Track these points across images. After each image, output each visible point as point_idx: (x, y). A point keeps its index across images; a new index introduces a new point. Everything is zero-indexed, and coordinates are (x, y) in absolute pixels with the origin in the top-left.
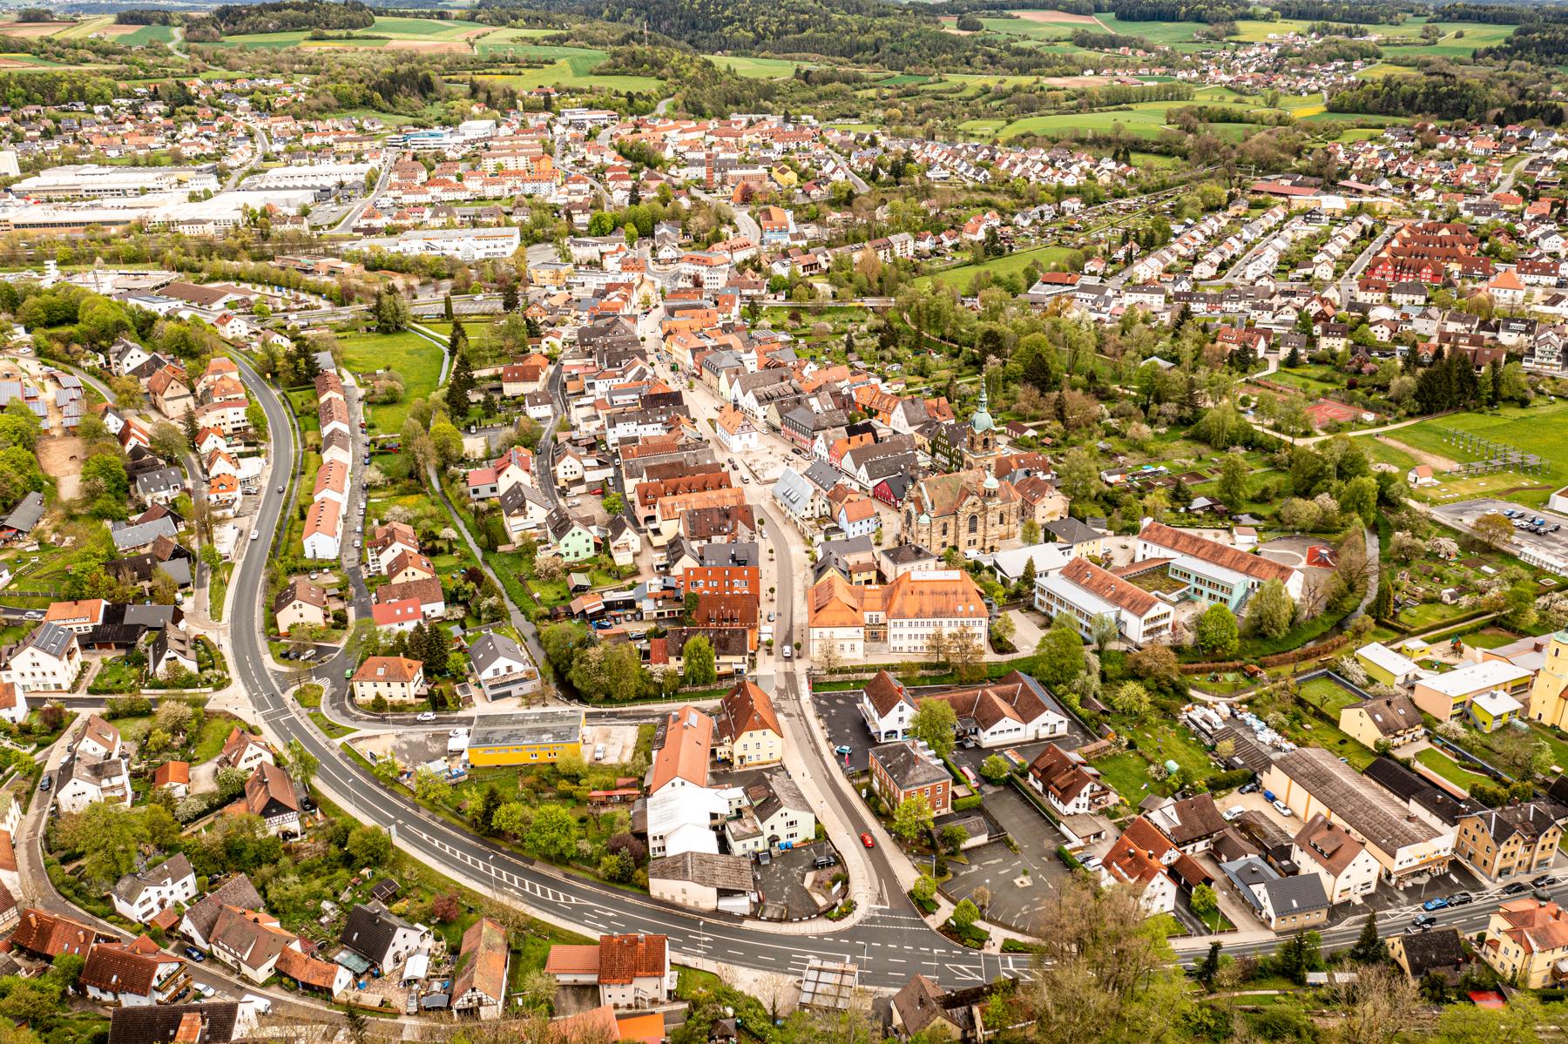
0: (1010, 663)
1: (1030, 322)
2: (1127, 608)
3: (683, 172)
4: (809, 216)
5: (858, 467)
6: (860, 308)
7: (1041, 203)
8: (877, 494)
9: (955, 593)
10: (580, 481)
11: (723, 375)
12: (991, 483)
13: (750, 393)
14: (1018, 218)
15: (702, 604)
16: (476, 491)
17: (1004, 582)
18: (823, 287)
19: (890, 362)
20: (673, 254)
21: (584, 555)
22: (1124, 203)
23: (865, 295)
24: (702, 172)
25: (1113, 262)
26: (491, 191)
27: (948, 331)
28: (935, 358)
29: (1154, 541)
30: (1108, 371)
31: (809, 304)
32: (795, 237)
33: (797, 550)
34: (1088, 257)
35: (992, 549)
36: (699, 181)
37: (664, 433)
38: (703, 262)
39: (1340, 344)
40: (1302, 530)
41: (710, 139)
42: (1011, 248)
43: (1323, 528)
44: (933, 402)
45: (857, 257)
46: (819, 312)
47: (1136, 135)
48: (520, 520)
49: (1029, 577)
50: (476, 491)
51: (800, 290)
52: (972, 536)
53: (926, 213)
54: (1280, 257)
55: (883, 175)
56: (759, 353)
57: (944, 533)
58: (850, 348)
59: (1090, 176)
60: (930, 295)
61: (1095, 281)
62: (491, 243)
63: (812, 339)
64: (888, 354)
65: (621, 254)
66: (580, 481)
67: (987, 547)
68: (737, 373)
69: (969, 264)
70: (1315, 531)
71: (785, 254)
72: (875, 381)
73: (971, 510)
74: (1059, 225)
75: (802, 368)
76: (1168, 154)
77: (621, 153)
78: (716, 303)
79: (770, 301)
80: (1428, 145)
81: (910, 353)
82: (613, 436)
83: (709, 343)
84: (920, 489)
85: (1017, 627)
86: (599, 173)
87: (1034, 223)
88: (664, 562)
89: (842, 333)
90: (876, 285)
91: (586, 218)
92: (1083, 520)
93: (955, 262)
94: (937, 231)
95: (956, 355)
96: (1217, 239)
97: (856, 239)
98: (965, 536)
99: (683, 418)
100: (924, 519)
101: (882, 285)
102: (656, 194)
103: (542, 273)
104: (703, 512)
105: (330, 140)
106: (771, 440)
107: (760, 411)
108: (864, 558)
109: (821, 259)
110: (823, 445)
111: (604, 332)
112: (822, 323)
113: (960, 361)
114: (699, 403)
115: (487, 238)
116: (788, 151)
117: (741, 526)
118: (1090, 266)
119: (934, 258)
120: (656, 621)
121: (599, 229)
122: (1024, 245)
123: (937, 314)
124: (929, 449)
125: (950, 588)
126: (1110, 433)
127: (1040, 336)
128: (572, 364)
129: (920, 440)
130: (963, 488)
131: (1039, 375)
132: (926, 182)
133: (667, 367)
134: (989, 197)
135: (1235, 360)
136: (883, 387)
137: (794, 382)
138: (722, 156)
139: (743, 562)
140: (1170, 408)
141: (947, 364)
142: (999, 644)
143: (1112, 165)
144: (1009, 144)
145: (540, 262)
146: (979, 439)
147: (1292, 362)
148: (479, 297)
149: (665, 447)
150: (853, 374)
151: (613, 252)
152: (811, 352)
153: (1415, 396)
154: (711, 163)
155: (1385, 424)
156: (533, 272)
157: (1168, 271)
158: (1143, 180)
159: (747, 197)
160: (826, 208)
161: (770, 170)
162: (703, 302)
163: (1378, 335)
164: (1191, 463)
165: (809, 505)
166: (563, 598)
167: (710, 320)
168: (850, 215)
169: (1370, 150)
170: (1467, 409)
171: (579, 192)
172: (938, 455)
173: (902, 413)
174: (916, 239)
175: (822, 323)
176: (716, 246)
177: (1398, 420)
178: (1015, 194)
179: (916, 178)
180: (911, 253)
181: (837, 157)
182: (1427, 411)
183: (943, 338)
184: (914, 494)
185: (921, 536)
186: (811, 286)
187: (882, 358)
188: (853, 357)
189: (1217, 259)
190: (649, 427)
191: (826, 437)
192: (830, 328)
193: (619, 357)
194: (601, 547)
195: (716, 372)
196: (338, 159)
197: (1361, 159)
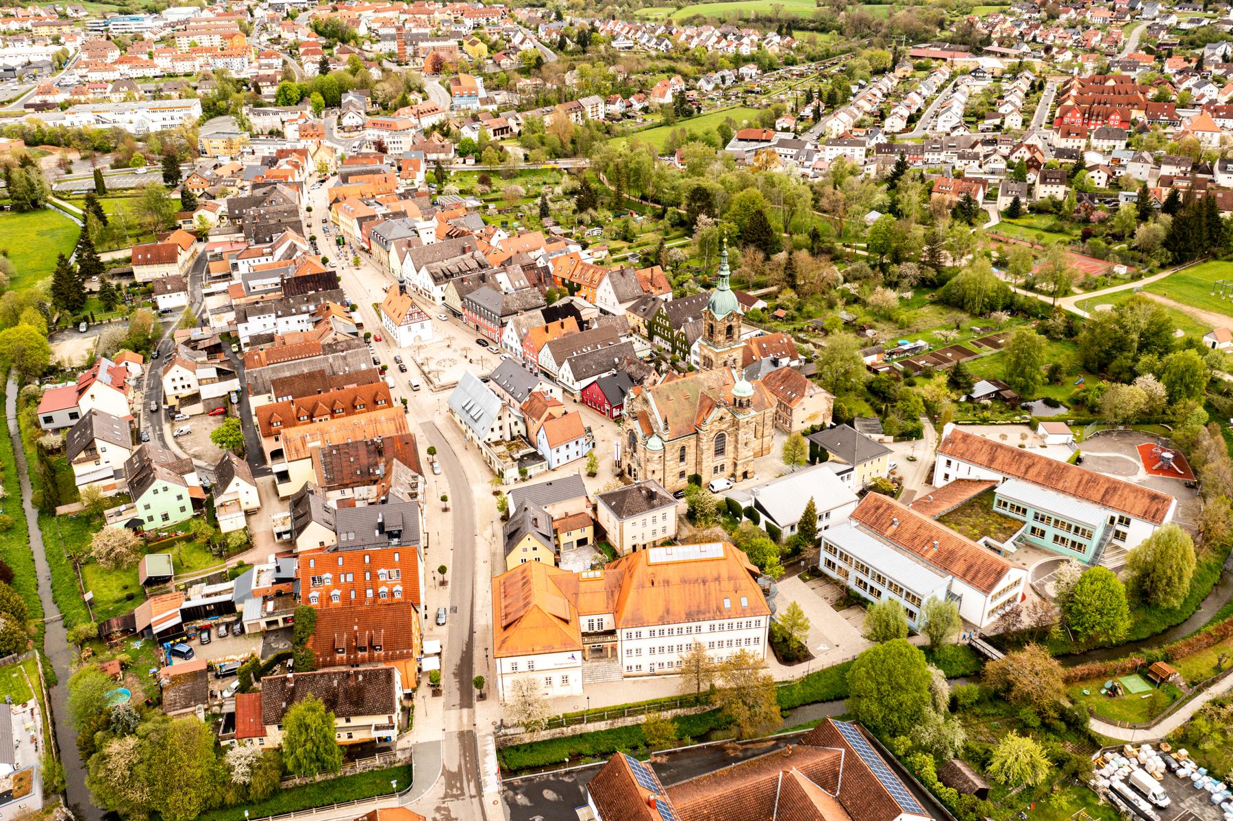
0: (807, 680)
1: (741, 177)
2: (963, 577)
3: (376, 47)
4: (494, 84)
5: (560, 364)
6: (553, 169)
7: (722, 68)
8: (587, 399)
9: (718, 579)
10: (195, 398)
11: (393, 248)
12: (744, 389)
13: (424, 271)
14: (702, 83)
15: (323, 626)
16: (48, 420)
17: (774, 533)
18: (514, 150)
19: (589, 226)
20: (357, 121)
21: (177, 517)
22: (796, 69)
24: (393, 46)
25: (802, 119)
26: (182, 67)
27: (650, 190)
28: (638, 221)
29: (962, 457)
30: (834, 231)
31: (500, 167)
32: (485, 101)
33: (481, 490)
34: (778, 116)
35: (745, 475)
36: (391, 55)
37: (310, 327)
38: (388, 127)
39: (1059, 192)
40: (1125, 422)
41: (403, 17)
42: (699, 109)
43: (1148, 419)
44: (647, 272)
45: (548, 120)
46: (511, 175)
47: (794, 15)
48: (90, 466)
49: (808, 524)
50: (48, 420)
51: (489, 153)
52: (720, 460)
53: (614, 78)
54: (965, 109)
55: (571, 45)
56: (440, 220)
57: (682, 459)
58: (544, 212)
59: (759, 47)
60: (628, 152)
61: (789, 136)
62: (167, 115)
63: (503, 204)
65: (301, 121)
66: (195, 398)
67: (739, 473)
68: (409, 245)
69: (660, 125)
70: (1141, 422)
71: (475, 118)
72: (575, 248)
73: (717, 427)
74: (741, 90)
75: (490, 236)
76: (824, 30)
77: (317, 31)
78: (400, 169)
79: (458, 165)
80: (1053, 16)
81: (610, 215)
82: (245, 332)
83: (380, 211)
84: (646, 401)
85: (813, 622)
86: (293, 50)
87: (717, 87)
88: (288, 527)
89: (536, 197)
90: (570, 147)
91: (274, 90)
92: (851, 423)
93: (647, 124)
94: (627, 95)
95: (660, 216)
96: (893, 96)
97: (547, 103)
98: (710, 461)
99: (335, 307)
100: (655, 443)
101: (575, 146)
102: (348, 67)
103: (216, 143)
104: (342, 450)
105: (28, 25)
106: (451, 329)
107: (437, 292)
108: (576, 506)
109: (512, 123)
110: (515, 335)
111: (257, 202)
112: (513, 186)
113: (666, 222)
114: (362, 285)
115: (163, 110)
116: (478, 26)
117: (398, 467)
118: (780, 123)
119: (625, 120)
120: (265, 634)
121: (285, 99)
122: (710, 107)
123: (637, 172)
124: (645, 332)
125: (709, 571)
127: (755, 192)
128: (219, 241)
129: (635, 320)
130: (704, 397)
131: (757, 234)
132: (611, 51)
133: (333, 241)
134: (673, 64)
135: (959, 211)
136: (583, 254)
137: (478, 254)
138: (414, 31)
139: (396, 535)
140: (910, 269)
141: (652, 226)
142: (786, 648)
143: (777, 39)
144: (683, 23)
145: (215, 137)
146: (721, 327)
147: (1013, 212)
148: (142, 170)
149: (306, 348)
150: (549, 241)
151: (292, 122)
152: (502, 217)
153: (1165, 244)
154: (401, 36)
155: (1139, 277)
156: (205, 142)
157: (859, 125)
158: (809, 49)
159: (438, 67)
160: (517, 75)
161: (461, 44)
162: (384, 167)
163: (1096, 180)
164: (953, 335)
165: (496, 424)
166: (130, 598)
167: (388, 186)
168: (539, 81)
169: (1004, 21)
170: (1215, 257)
171: (270, 66)
172: (657, 339)
173: (610, 288)
174: (607, 102)
175: (513, 186)
176: (401, 110)
177: (1151, 272)
178: (695, 61)
179: (602, 47)
180: (602, 116)
181: (525, 31)
182: (1179, 260)
183: (644, 198)
184: (638, 407)
185: (650, 467)
186: (502, 149)
187: (581, 222)
188: (548, 222)
189: (906, 113)
190: (293, 320)
191: (518, 325)
192: (523, 191)
193: (270, 231)
194: (204, 506)
195: (385, 244)
196: (34, 42)
197: (998, 28)
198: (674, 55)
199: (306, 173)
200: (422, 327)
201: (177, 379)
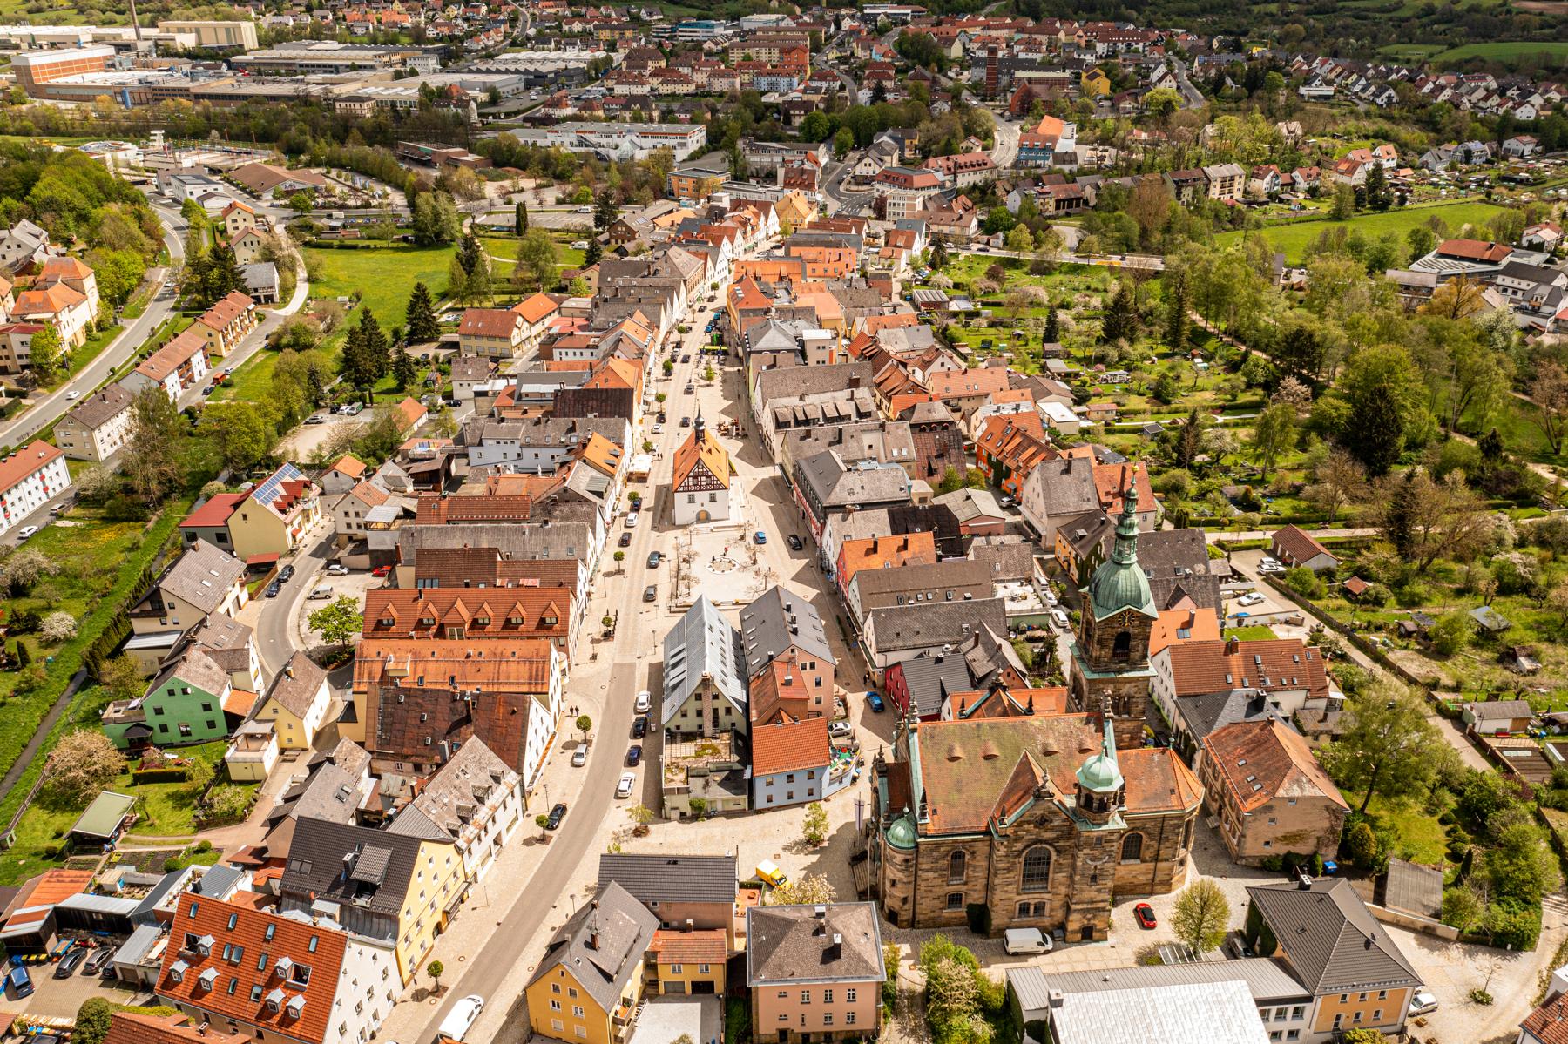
23: (1131, 250)
26: (720, 85)
42: (1403, 200)
64: (1113, 353)
67: (1075, 923)
74: (1493, 174)
115: (654, 135)
126: (1509, 586)
138: (1022, 56)
161: (1078, 76)
187: (1101, 359)
198: (1396, 113)
199: (760, 235)
200: (713, 499)
201: (352, 514)
